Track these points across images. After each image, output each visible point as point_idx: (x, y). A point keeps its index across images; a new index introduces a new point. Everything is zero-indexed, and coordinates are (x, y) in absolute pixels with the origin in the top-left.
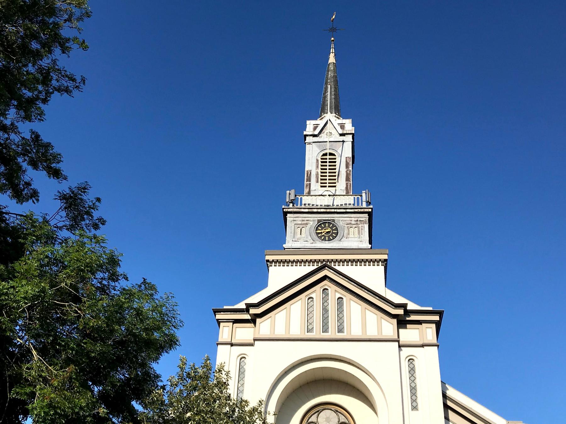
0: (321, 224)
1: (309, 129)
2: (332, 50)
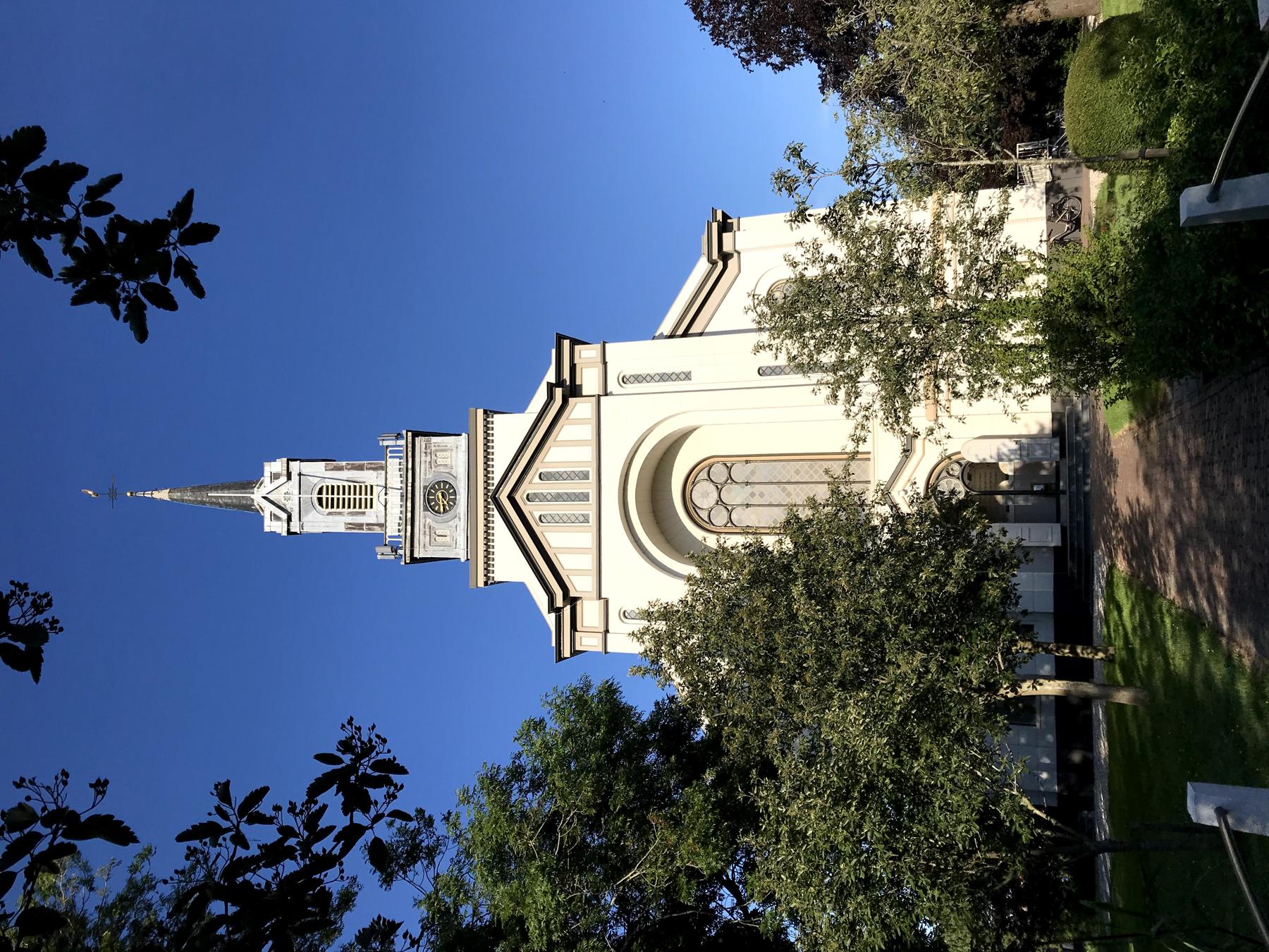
0: (430, 505)
1: (280, 528)
2: (148, 494)
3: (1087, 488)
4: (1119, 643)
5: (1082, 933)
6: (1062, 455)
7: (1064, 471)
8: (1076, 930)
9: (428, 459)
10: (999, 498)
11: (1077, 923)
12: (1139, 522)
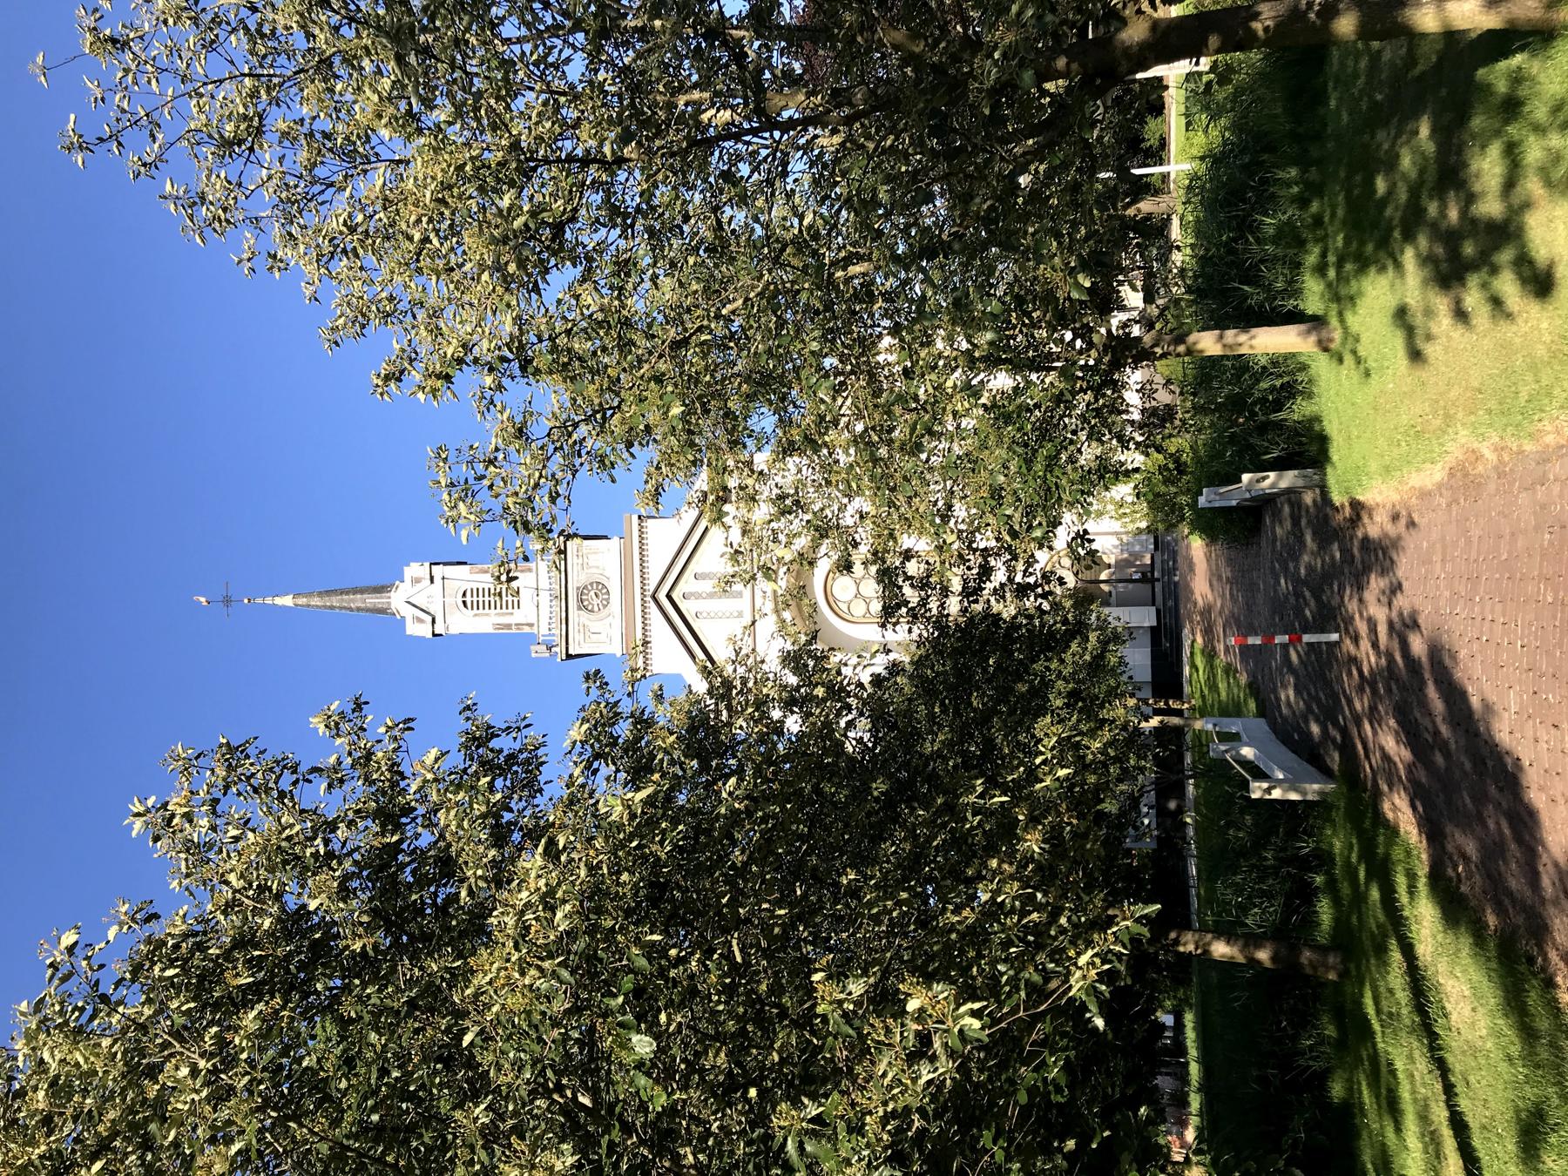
0: (582, 606)
1: (425, 631)
2: (269, 601)
3: (1177, 579)
4: (1197, 695)
5: (1180, 1000)
6: (1156, 548)
7: (1158, 565)
8: (1175, 997)
9: (580, 561)
10: (1103, 586)
11: (1176, 990)
12: (1207, 610)
